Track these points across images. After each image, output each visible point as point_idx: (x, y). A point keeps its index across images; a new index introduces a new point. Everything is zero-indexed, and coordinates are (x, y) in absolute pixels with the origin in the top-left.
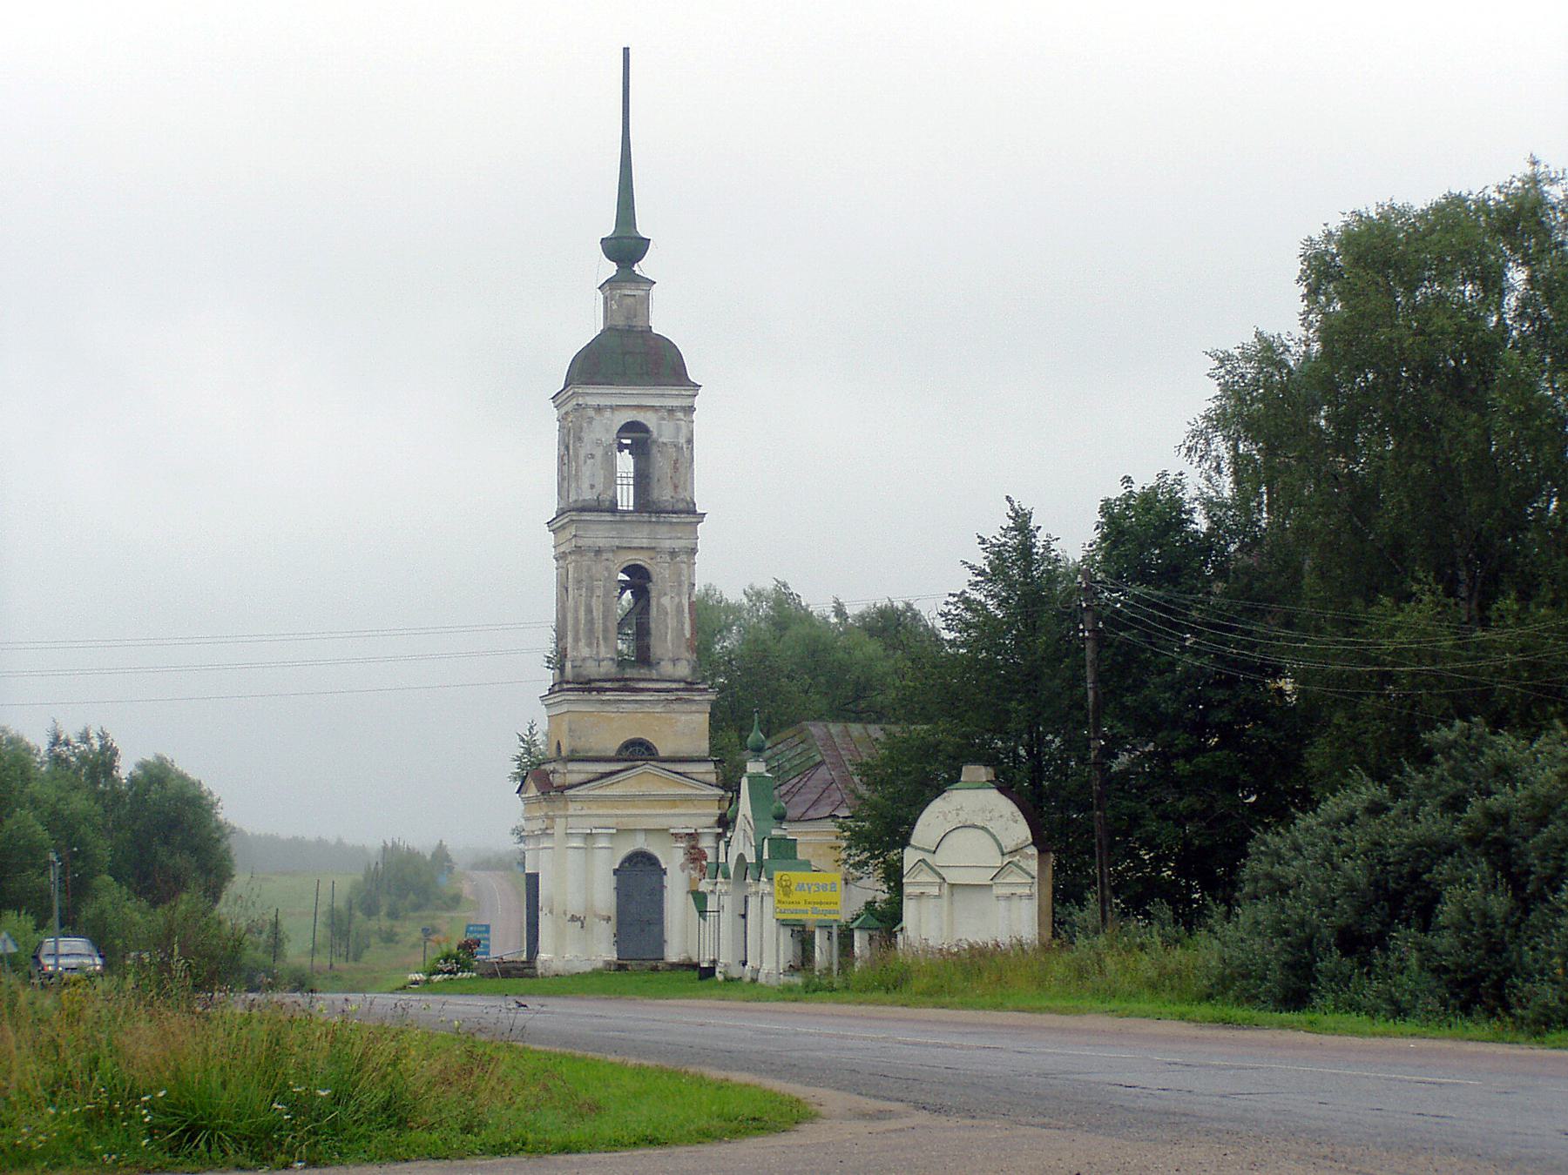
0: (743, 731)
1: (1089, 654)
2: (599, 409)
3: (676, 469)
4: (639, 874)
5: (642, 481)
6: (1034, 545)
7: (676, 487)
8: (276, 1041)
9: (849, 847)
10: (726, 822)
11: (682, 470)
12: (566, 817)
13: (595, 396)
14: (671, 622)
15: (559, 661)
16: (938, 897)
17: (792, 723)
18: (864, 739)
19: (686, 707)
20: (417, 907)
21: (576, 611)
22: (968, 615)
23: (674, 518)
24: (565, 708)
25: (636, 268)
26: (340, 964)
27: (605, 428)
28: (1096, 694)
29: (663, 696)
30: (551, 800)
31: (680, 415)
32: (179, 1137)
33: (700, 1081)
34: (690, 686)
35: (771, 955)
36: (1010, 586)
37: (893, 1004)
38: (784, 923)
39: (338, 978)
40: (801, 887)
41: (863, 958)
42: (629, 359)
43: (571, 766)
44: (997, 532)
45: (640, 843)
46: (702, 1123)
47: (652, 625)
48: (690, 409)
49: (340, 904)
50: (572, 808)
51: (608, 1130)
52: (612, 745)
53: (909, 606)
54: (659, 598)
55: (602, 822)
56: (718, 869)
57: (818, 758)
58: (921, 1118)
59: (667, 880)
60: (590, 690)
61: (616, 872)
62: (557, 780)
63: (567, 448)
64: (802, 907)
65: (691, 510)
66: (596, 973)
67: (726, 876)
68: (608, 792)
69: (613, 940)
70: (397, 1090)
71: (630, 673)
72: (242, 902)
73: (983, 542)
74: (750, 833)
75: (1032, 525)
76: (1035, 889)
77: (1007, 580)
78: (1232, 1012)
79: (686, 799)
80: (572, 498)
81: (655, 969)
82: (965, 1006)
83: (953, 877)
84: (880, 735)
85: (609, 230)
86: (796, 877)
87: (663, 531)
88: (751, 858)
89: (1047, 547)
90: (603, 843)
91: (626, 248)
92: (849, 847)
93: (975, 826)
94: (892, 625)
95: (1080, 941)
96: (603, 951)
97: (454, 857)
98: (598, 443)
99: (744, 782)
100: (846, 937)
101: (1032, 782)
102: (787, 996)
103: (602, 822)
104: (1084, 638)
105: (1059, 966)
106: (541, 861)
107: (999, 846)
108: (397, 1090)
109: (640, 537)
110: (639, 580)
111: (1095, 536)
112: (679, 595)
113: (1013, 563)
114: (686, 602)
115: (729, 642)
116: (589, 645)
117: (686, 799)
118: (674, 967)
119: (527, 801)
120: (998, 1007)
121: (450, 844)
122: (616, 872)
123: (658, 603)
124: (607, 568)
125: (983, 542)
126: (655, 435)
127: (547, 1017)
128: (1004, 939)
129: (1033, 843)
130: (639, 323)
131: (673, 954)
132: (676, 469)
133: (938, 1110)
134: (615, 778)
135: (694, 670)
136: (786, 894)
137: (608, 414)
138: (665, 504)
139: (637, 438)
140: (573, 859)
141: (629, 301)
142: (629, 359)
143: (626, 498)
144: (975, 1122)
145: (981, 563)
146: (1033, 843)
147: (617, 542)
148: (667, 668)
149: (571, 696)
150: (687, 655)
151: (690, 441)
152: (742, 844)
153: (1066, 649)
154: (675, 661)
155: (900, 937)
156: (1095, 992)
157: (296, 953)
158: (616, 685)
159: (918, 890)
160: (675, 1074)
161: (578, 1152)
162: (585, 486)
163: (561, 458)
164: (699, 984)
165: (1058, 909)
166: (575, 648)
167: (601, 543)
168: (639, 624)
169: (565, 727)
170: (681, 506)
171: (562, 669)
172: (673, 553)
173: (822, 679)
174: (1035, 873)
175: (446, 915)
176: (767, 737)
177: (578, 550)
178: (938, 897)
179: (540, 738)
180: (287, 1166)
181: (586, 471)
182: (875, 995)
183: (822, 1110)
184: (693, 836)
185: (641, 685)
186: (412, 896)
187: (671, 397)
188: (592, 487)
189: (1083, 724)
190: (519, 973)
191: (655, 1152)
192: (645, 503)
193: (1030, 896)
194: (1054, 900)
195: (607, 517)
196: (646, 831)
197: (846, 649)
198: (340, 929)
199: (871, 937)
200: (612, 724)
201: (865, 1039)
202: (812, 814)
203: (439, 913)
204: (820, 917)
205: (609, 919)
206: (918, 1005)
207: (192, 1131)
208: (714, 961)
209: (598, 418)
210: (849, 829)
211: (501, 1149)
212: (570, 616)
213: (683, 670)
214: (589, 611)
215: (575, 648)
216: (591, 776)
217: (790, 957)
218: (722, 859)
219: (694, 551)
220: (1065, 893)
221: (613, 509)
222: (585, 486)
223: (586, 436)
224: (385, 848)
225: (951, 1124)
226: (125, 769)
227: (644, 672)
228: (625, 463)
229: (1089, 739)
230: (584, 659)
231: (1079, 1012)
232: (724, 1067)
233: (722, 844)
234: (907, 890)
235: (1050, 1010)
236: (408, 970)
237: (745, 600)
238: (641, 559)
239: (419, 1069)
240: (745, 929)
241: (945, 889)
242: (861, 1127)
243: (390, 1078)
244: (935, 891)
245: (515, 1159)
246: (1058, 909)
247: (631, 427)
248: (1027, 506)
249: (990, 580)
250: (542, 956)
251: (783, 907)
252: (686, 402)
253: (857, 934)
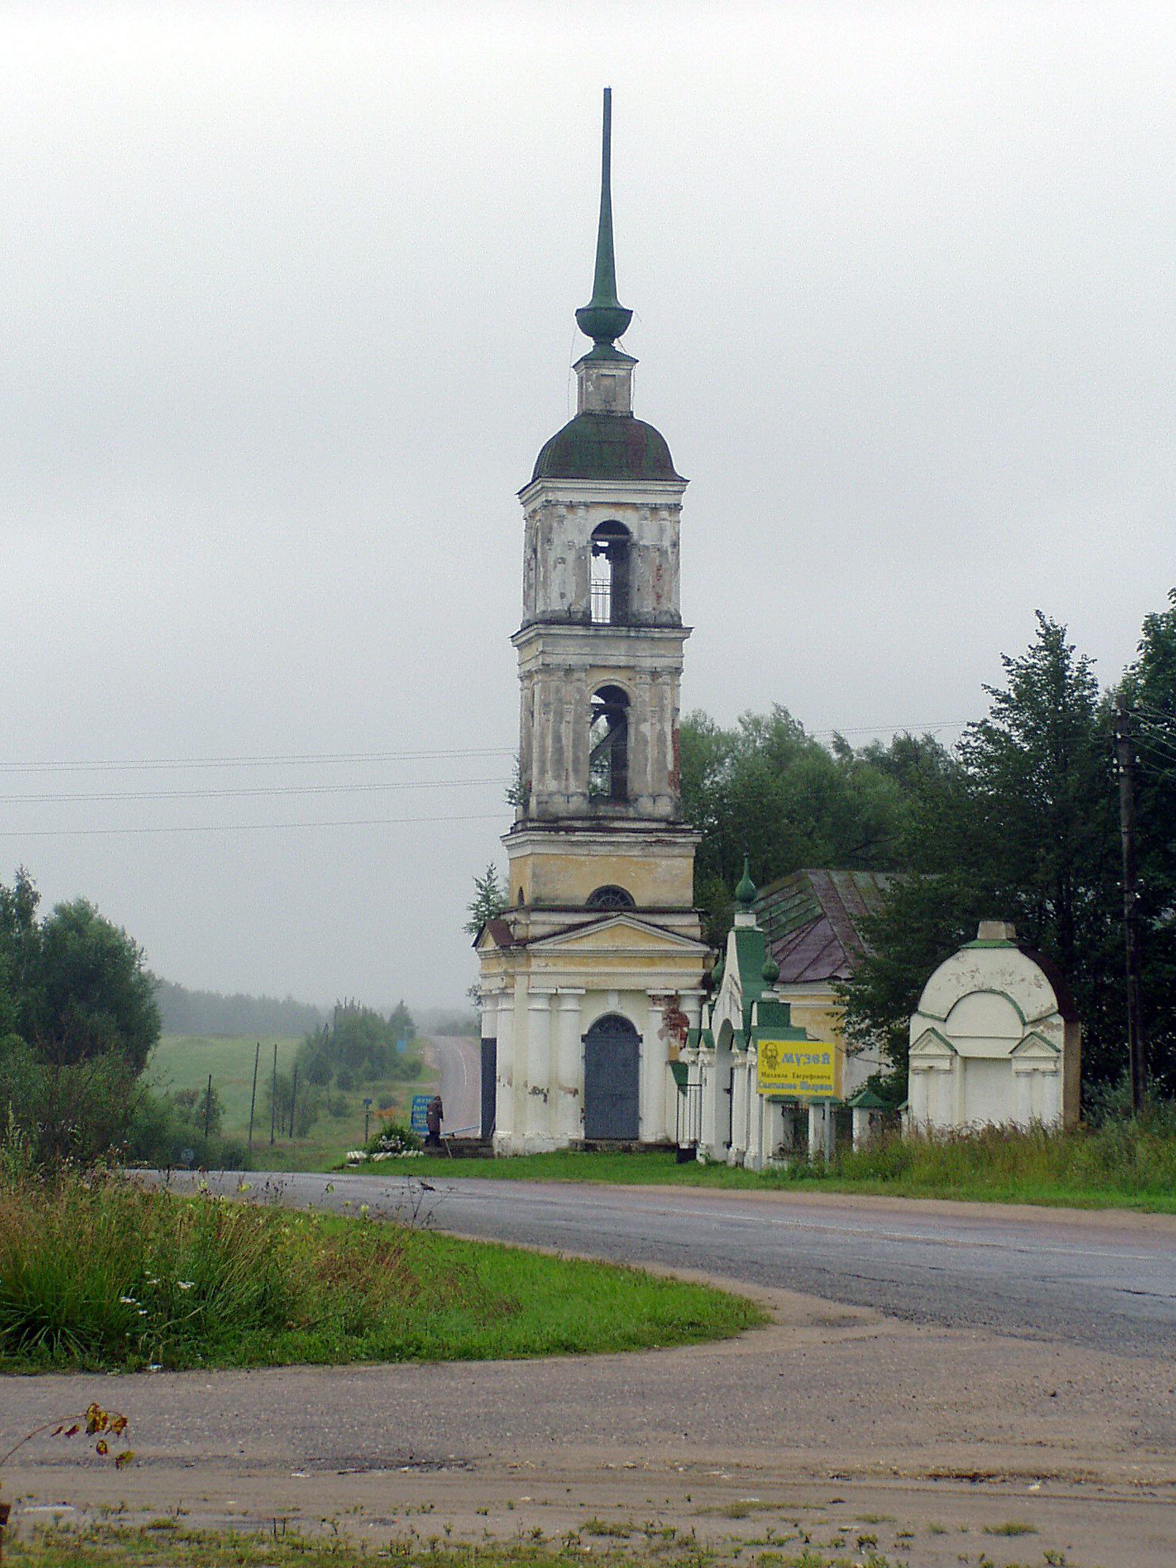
0: (732, 878)
1: (1124, 795)
2: (571, 506)
3: (659, 577)
4: (610, 1042)
5: (620, 589)
6: (1067, 668)
7: (659, 597)
8: (128, 1225)
9: (849, 1014)
10: (710, 983)
11: (666, 577)
12: (529, 974)
13: (568, 491)
14: (652, 752)
15: (522, 795)
16: (950, 1072)
17: (793, 869)
18: (866, 889)
19: (668, 850)
20: (373, 1077)
21: (543, 737)
22: (990, 748)
23: (656, 633)
24: (528, 850)
25: (616, 343)
26: (283, 1139)
27: (579, 528)
28: (1132, 841)
29: (641, 837)
30: (511, 955)
31: (664, 514)
32: (16, 1334)
33: (641, 1278)
34: (672, 826)
35: (758, 1137)
36: (1040, 715)
37: (889, 1194)
38: (774, 1100)
39: (280, 1155)
40: (788, 1058)
41: (862, 1142)
42: (606, 446)
43: (535, 917)
44: (1025, 652)
45: (612, 1005)
46: (630, 1328)
47: (630, 756)
48: (676, 508)
49: (285, 1071)
50: (536, 965)
51: (519, 1335)
52: (581, 892)
53: (929, 740)
54: (638, 723)
55: (564, 980)
56: (700, 1037)
57: (819, 910)
58: (890, 1325)
59: (643, 1049)
60: (557, 830)
61: (584, 1039)
62: (518, 932)
63: (535, 551)
64: (790, 1081)
65: (675, 624)
66: (561, 1153)
67: (710, 1045)
68: (576, 946)
69: (580, 1115)
70: (272, 1282)
71: (603, 810)
72: (172, 1068)
73: (1008, 663)
74: (738, 996)
75: (1065, 644)
76: (1061, 1064)
77: (1035, 705)
78: (1068, 1196)
79: (667, 956)
80: (540, 608)
81: (627, 1150)
82: (971, 1197)
83: (965, 1049)
84: (888, 887)
85: (585, 299)
86: (784, 1046)
87: (643, 648)
88: (738, 1025)
89: (1082, 670)
90: (570, 1004)
91: (604, 321)
92: (849, 1014)
93: (992, 991)
94: (910, 759)
95: (1109, 1125)
96: (565, 1126)
97: (416, 1021)
98: (570, 545)
99: (732, 937)
100: (842, 1117)
101: (1061, 941)
102: (770, 1182)
103: (564, 980)
104: (1118, 775)
105: (1084, 1153)
106: (499, 1025)
107: (1020, 1013)
108: (272, 1282)
109: (618, 654)
110: (615, 703)
111: (1139, 657)
112: (661, 720)
113: (1043, 687)
114: (668, 730)
115: (722, 776)
116: (557, 777)
117: (667, 956)
118: (650, 1148)
119: (485, 956)
120: (1008, 1199)
121: (411, 1006)
122: (584, 1039)
123: (637, 729)
124: (579, 690)
125: (1008, 663)
126: (635, 536)
127: (459, 1197)
128: (1023, 1121)
129: (1059, 1012)
130: (618, 408)
131: (649, 1133)
132: (659, 577)
133: (909, 1317)
134: (583, 931)
135: (677, 808)
136: (771, 1066)
137: (581, 512)
138: (643, 615)
139: (615, 540)
140: (536, 1024)
141: (607, 382)
142: (606, 446)
143: (601, 610)
144: (949, 1332)
145: (1007, 688)
146: (1059, 1012)
147: (590, 660)
148: (646, 806)
149: (537, 836)
150: (669, 791)
151: (675, 545)
152: (728, 1008)
153: (1100, 786)
154: (655, 798)
155: (904, 1118)
156: (1123, 1186)
157: (232, 1126)
158: (587, 824)
159: (925, 1064)
160: (614, 1270)
161: (481, 1358)
162: (555, 594)
163: (528, 563)
164: (678, 1167)
165: (1087, 1086)
166: (541, 781)
167: (572, 660)
168: (615, 753)
169: (528, 872)
170: (665, 619)
171: (526, 805)
172: (655, 674)
173: (828, 820)
174: (1061, 1047)
175: (405, 1085)
176: (758, 886)
177: (546, 668)
178: (950, 1072)
179: (500, 884)
180: (140, 1369)
181: (556, 577)
182: (870, 1183)
183: (777, 1316)
184: (674, 1000)
185: (617, 824)
186: (366, 1064)
187: (654, 493)
188: (563, 596)
189: (1117, 875)
190: (476, 1152)
191: (568, 1361)
192: (623, 616)
193: (1055, 1073)
194: (1083, 1076)
195: (579, 631)
196: (620, 992)
197: (858, 788)
198: (287, 1102)
199: (872, 1118)
200: (582, 870)
201: (846, 1233)
202: (810, 974)
203: (397, 1084)
204: (812, 1093)
205: (576, 1092)
206: (916, 1195)
207: (32, 1326)
208: (695, 1142)
209: (570, 517)
210: (848, 992)
211: (390, 1354)
212: (535, 744)
213: (665, 808)
214: (558, 739)
215: (541, 781)
216: (558, 928)
217: (781, 1137)
218: (705, 1026)
219: (678, 671)
220: (1095, 1073)
221: (586, 621)
222: (555, 594)
223: (557, 539)
224: (337, 1009)
225: (922, 1333)
226: (42, 914)
227: (620, 810)
228: (601, 568)
229: (1121, 891)
230: (551, 795)
231: (1100, 1206)
232: (674, 1263)
233: (706, 1008)
234: (914, 1063)
235: (1066, 1203)
236: (347, 1147)
237: (741, 729)
238: (618, 680)
239: (303, 1257)
240: (714, 1105)
241: (958, 1062)
242: (816, 1335)
243: (263, 1269)
244: (945, 1065)
245: (406, 1366)
246: (1087, 1086)
247: (609, 528)
248: (1060, 623)
249: (1016, 708)
250: (500, 1133)
251: (767, 1080)
252: (670, 500)
253: (856, 1114)
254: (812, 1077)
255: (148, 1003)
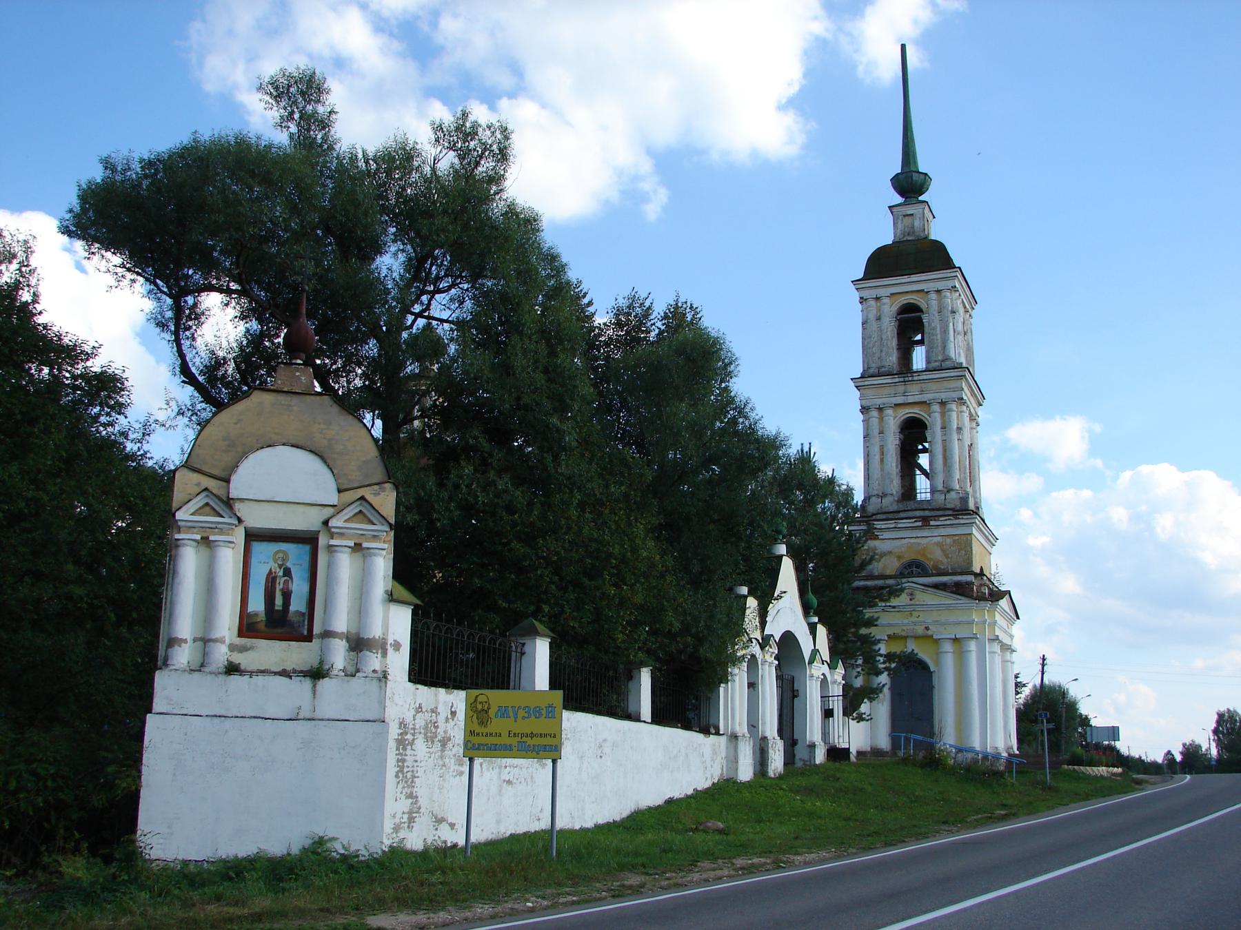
40: (503, 712)
42: (912, 257)
91: (910, 185)
226: (1178, 758)
251: (476, 740)
254: (532, 735)
255: (1058, 417)
